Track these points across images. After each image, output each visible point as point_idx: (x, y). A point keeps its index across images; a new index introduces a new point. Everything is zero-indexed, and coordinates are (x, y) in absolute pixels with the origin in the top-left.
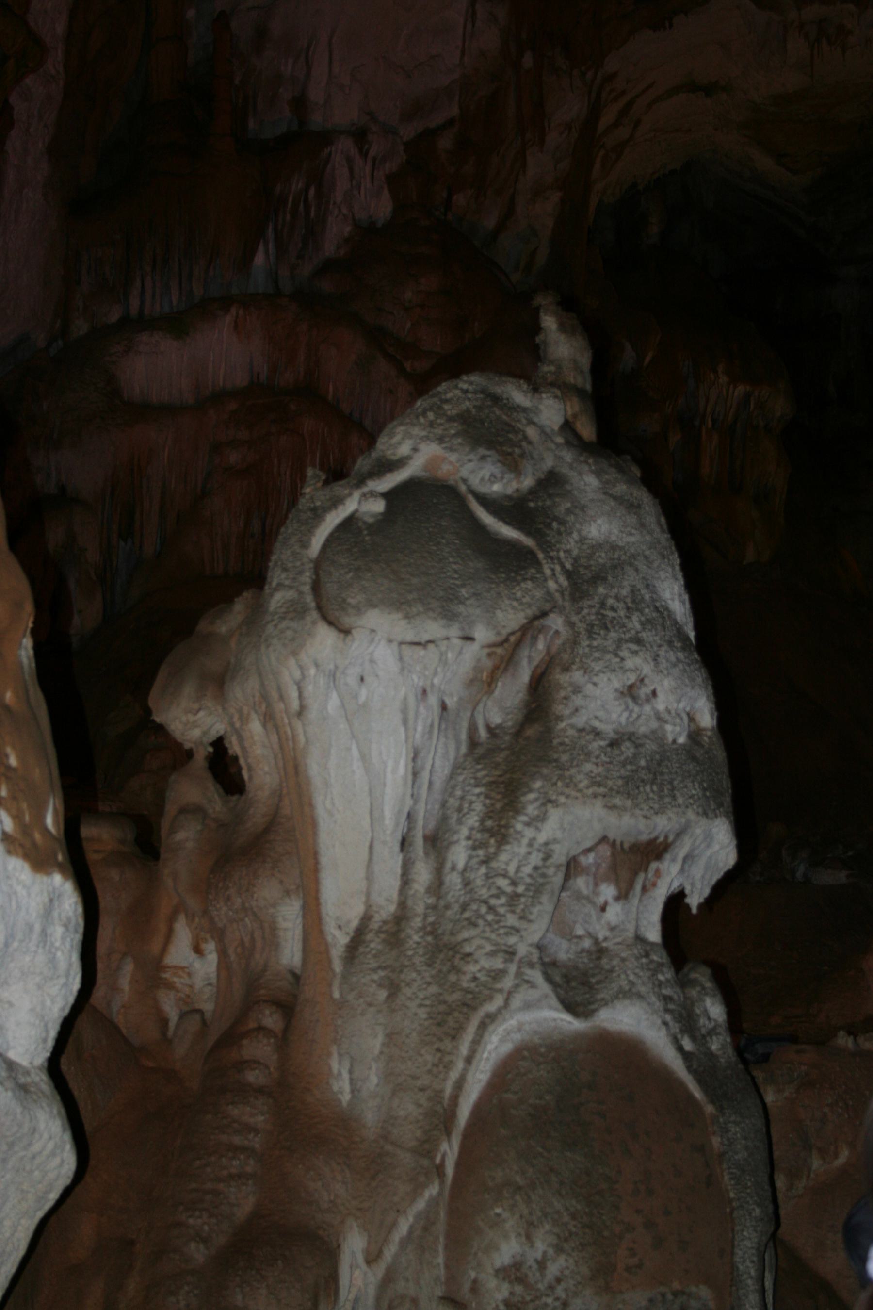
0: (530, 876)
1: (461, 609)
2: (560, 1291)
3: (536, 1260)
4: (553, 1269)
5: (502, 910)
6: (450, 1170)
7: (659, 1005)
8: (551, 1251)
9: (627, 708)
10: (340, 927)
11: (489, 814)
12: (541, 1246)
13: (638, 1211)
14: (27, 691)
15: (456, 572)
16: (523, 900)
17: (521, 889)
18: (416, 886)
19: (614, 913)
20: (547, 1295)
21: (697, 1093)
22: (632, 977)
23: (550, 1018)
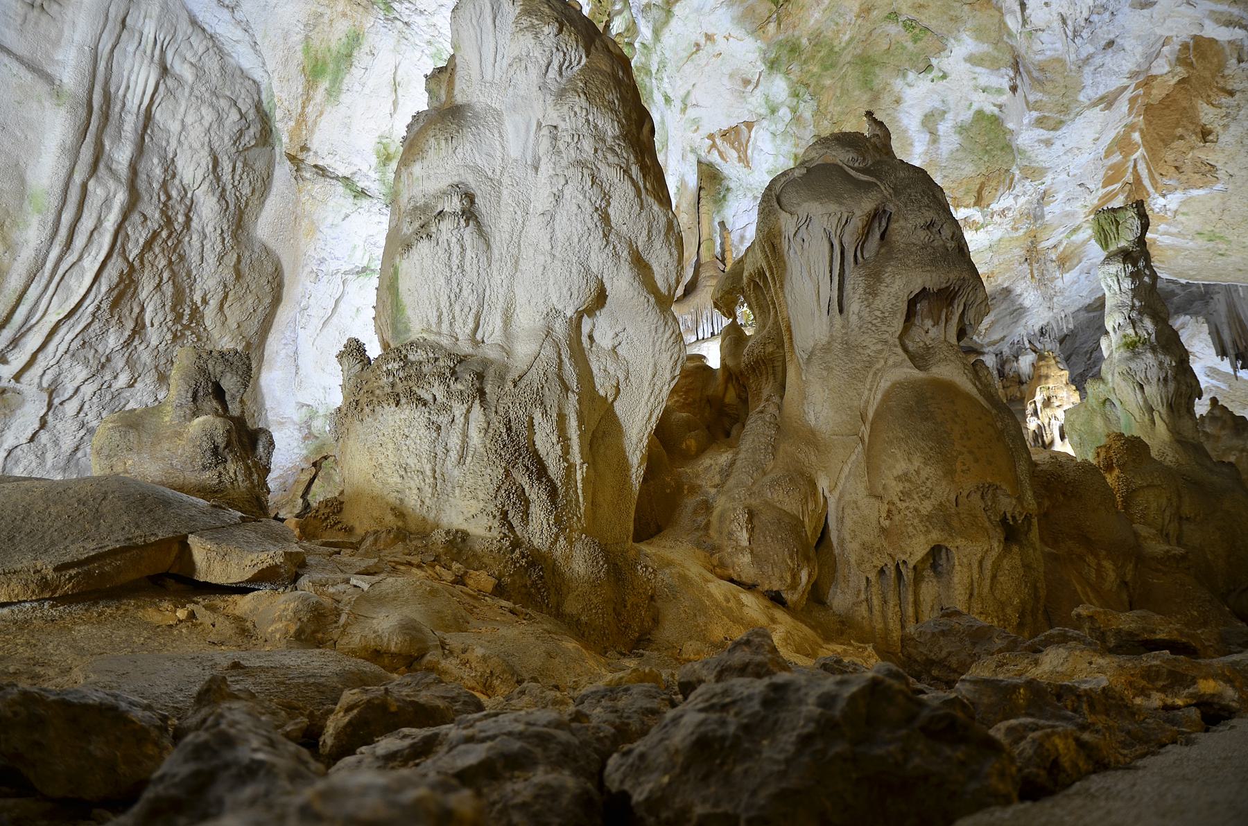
2: (928, 483)
4: (924, 474)
6: (867, 440)
11: (869, 286)
12: (917, 462)
18: (224, 178)
19: (933, 332)
23: (910, 372)
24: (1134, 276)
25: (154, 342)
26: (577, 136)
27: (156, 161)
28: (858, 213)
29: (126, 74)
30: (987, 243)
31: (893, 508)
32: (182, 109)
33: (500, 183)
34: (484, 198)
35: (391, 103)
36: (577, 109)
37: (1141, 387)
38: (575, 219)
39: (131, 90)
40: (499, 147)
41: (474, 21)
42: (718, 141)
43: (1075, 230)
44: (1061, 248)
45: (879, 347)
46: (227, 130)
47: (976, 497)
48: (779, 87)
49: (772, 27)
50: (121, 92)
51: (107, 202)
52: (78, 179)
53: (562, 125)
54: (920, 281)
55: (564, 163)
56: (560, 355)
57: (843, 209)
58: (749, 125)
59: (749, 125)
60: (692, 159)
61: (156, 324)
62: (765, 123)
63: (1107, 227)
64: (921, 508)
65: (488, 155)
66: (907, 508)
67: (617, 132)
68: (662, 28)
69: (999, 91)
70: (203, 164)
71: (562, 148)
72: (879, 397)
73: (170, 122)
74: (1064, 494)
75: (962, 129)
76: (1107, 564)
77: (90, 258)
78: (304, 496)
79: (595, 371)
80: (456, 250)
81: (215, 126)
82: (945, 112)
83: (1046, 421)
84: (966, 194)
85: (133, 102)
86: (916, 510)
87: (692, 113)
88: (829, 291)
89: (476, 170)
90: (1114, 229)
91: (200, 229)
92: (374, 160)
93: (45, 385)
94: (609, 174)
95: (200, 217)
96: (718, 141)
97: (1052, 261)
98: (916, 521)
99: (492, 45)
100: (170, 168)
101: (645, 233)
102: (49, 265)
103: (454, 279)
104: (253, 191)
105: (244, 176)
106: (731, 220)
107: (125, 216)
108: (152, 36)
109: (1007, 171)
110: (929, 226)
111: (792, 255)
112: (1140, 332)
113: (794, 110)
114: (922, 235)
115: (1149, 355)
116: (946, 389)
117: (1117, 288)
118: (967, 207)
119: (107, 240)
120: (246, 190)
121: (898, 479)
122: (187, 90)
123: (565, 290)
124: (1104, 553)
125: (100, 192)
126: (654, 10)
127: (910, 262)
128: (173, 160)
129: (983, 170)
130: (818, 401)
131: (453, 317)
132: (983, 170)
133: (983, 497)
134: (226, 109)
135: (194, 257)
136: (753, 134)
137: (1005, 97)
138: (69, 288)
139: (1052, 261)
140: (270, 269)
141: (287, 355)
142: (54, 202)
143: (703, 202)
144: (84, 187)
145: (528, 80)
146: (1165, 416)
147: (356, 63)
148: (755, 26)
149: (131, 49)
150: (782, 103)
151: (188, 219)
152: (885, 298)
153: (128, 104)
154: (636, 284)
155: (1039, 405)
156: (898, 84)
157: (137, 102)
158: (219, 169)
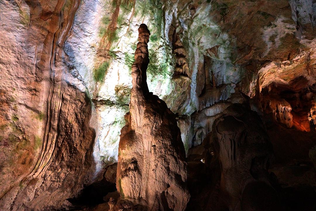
25: (66, 160)
26: (160, 148)
27: (63, 121)
29: (55, 104)
30: (293, 68)
32: (68, 106)
33: (143, 156)
34: (139, 161)
36: (160, 141)
38: (160, 172)
39: (56, 107)
40: (142, 146)
41: (135, 112)
42: (209, 51)
46: (79, 107)
48: (225, 36)
49: (222, 22)
50: (54, 108)
51: (53, 137)
52: (46, 135)
53: (157, 146)
55: (158, 156)
56: (159, 203)
58: (217, 47)
59: (217, 47)
60: (202, 55)
61: (66, 156)
62: (222, 46)
65: (140, 149)
67: (170, 144)
68: (190, 25)
69: (293, 29)
70: (74, 117)
71: (157, 152)
73: (65, 110)
75: (282, 39)
77: (51, 150)
78: (104, 176)
79: (168, 203)
80: (133, 178)
81: (76, 108)
82: (276, 35)
83: (314, 118)
84: (285, 57)
85: (57, 110)
87: (201, 45)
88: (231, 153)
89: (137, 153)
91: (74, 131)
93: (43, 176)
94: (168, 157)
95: (74, 129)
96: (209, 51)
99: (139, 118)
100: (66, 121)
101: (178, 170)
102: (42, 156)
103: (133, 185)
104: (86, 117)
105: (83, 115)
106: (214, 70)
107: (57, 138)
108: (60, 92)
109: (298, 49)
113: (230, 41)
118: (285, 60)
119: (54, 145)
120: (84, 118)
122: (69, 101)
123: (159, 189)
125: (51, 135)
126: (188, 21)
128: (67, 118)
129: (290, 50)
131: (134, 194)
132: (290, 50)
134: (78, 103)
135: (73, 138)
136: (219, 49)
137: (295, 30)
138: (47, 158)
140: (91, 133)
141: (97, 147)
142: (42, 142)
143: (206, 66)
144: (48, 135)
145: (148, 130)
147: (108, 71)
148: (217, 21)
149: (55, 97)
150: (227, 40)
151: (71, 130)
153: (56, 110)
154: (177, 185)
155: (312, 114)
156: (261, 30)
157: (58, 109)
158: (77, 117)
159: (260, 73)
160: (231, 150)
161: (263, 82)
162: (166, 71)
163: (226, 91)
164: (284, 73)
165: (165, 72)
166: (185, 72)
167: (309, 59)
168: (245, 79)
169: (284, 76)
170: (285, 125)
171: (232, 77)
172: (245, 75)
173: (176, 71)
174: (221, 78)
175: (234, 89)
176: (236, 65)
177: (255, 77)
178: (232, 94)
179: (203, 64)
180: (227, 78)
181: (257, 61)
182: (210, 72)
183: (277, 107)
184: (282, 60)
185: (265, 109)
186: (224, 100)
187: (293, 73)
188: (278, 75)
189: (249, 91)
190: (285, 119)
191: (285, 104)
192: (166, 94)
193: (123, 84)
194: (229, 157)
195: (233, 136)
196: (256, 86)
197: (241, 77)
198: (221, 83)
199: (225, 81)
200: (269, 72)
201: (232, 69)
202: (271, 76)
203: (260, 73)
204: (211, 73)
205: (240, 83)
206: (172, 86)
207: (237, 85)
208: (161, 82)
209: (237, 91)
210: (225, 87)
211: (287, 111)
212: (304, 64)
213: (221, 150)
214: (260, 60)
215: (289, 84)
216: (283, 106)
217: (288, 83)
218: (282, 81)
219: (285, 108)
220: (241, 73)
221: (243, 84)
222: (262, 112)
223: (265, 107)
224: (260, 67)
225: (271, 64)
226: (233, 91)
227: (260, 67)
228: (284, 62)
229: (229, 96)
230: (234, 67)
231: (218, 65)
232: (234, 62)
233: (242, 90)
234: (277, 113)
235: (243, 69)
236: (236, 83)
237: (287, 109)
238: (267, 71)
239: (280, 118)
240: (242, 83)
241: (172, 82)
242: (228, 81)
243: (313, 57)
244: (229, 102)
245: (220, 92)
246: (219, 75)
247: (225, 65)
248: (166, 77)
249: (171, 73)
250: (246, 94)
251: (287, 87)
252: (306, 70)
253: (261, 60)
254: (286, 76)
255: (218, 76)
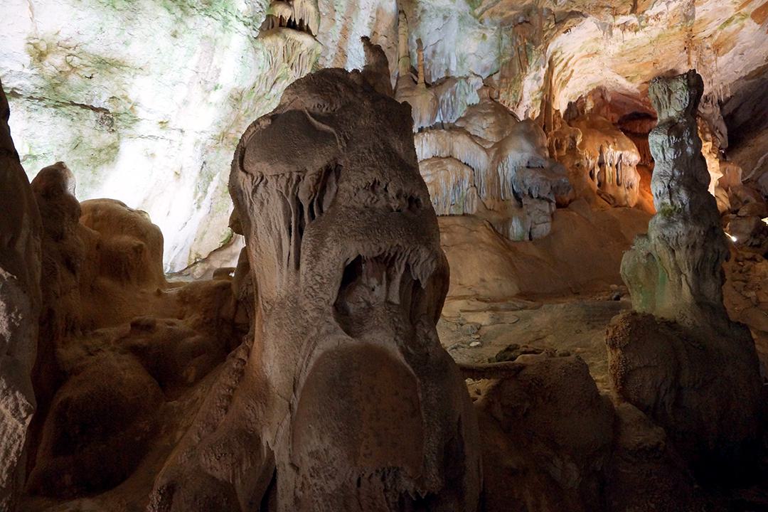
0: (329, 275)
1: (297, 159)
3: (324, 449)
5: (317, 291)
7: (392, 332)
8: (330, 446)
9: (370, 196)
10: (267, 302)
12: (327, 442)
13: (371, 428)
14: (280, 239)
15: (296, 144)
16: (325, 285)
17: (325, 281)
20: (329, 466)
21: (413, 373)
22: (380, 319)
23: (340, 339)
24: (678, 146)
28: (310, 171)
30: (647, 41)
31: (305, 482)
35: (28, 10)
37: (673, 251)
43: (728, 22)
44: (716, 37)
45: (315, 314)
47: (377, 479)
54: (354, 249)
57: (293, 169)
63: (660, 96)
64: (326, 487)
66: (315, 485)
72: (311, 364)
74: (544, 398)
76: (571, 466)
86: (322, 489)
90: (666, 97)
92: (27, 59)
97: (708, 48)
98: (320, 500)
110: (373, 187)
111: (256, 210)
112: (675, 202)
114: (364, 197)
115: (681, 225)
116: (376, 356)
117: (662, 156)
118: (624, 14)
121: (311, 454)
124: (569, 457)
127: (347, 230)
130: (273, 355)
133: (383, 479)
139: (708, 48)
143: (401, 24)
146: (690, 280)
152: (325, 262)
159: (555, 53)
160: (287, 241)
161: (567, 81)
162: (229, 10)
163: (455, 98)
164: (625, 58)
165: (225, 10)
166: (302, 21)
167: (691, 14)
168: (510, 64)
169: (626, 66)
170: (615, 202)
171: (475, 58)
172: (510, 52)
173: (272, 15)
174: (443, 61)
175: (478, 91)
176: (487, 22)
177: (537, 59)
178: (471, 107)
179: (393, 15)
180: (459, 60)
181: (545, 12)
182: (414, 41)
183: (601, 152)
184: (615, 15)
185: (565, 154)
186: (448, 123)
187: (649, 58)
188: (610, 64)
189: (521, 100)
190: (619, 184)
191: (623, 145)
192: (236, 85)
193: (57, 34)
194: (280, 257)
195: (288, 180)
196: (542, 90)
197: (500, 57)
198: (443, 75)
199: (453, 68)
200: (584, 53)
201: (472, 34)
202: (589, 64)
203: (555, 53)
204: (416, 45)
205: (496, 78)
206: (256, 59)
207: (487, 84)
208: (211, 44)
209: (485, 98)
210: (452, 85)
211: (628, 164)
212: (677, 29)
213: (255, 233)
214: (553, 9)
215: (639, 92)
216: (616, 150)
217: (638, 88)
218: (622, 81)
219: (621, 155)
220: (499, 47)
221: (504, 80)
222: (545, 158)
223: (565, 149)
224: (553, 29)
225: (586, 25)
226: (474, 99)
227: (553, 29)
228: (621, 20)
229: (461, 112)
230: (479, 28)
231: (438, 22)
232: (477, 12)
233: (499, 97)
234: (600, 167)
235: (504, 35)
236: (485, 76)
237: (627, 158)
238: (577, 49)
239: (607, 181)
240: (502, 77)
241: (256, 49)
242: (463, 68)
243: (704, 13)
244: (460, 128)
245: (436, 98)
246: (438, 50)
247: (454, 23)
248: (232, 28)
249: (255, 19)
250: (513, 108)
251: (636, 102)
252: (685, 53)
253: (557, 8)
254: (630, 66)
255: (434, 52)
